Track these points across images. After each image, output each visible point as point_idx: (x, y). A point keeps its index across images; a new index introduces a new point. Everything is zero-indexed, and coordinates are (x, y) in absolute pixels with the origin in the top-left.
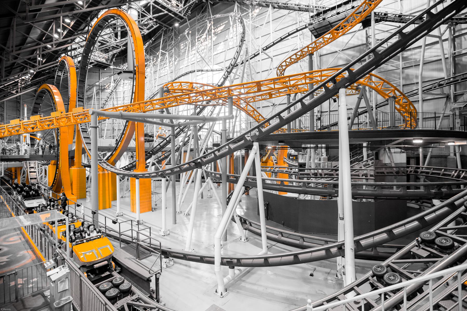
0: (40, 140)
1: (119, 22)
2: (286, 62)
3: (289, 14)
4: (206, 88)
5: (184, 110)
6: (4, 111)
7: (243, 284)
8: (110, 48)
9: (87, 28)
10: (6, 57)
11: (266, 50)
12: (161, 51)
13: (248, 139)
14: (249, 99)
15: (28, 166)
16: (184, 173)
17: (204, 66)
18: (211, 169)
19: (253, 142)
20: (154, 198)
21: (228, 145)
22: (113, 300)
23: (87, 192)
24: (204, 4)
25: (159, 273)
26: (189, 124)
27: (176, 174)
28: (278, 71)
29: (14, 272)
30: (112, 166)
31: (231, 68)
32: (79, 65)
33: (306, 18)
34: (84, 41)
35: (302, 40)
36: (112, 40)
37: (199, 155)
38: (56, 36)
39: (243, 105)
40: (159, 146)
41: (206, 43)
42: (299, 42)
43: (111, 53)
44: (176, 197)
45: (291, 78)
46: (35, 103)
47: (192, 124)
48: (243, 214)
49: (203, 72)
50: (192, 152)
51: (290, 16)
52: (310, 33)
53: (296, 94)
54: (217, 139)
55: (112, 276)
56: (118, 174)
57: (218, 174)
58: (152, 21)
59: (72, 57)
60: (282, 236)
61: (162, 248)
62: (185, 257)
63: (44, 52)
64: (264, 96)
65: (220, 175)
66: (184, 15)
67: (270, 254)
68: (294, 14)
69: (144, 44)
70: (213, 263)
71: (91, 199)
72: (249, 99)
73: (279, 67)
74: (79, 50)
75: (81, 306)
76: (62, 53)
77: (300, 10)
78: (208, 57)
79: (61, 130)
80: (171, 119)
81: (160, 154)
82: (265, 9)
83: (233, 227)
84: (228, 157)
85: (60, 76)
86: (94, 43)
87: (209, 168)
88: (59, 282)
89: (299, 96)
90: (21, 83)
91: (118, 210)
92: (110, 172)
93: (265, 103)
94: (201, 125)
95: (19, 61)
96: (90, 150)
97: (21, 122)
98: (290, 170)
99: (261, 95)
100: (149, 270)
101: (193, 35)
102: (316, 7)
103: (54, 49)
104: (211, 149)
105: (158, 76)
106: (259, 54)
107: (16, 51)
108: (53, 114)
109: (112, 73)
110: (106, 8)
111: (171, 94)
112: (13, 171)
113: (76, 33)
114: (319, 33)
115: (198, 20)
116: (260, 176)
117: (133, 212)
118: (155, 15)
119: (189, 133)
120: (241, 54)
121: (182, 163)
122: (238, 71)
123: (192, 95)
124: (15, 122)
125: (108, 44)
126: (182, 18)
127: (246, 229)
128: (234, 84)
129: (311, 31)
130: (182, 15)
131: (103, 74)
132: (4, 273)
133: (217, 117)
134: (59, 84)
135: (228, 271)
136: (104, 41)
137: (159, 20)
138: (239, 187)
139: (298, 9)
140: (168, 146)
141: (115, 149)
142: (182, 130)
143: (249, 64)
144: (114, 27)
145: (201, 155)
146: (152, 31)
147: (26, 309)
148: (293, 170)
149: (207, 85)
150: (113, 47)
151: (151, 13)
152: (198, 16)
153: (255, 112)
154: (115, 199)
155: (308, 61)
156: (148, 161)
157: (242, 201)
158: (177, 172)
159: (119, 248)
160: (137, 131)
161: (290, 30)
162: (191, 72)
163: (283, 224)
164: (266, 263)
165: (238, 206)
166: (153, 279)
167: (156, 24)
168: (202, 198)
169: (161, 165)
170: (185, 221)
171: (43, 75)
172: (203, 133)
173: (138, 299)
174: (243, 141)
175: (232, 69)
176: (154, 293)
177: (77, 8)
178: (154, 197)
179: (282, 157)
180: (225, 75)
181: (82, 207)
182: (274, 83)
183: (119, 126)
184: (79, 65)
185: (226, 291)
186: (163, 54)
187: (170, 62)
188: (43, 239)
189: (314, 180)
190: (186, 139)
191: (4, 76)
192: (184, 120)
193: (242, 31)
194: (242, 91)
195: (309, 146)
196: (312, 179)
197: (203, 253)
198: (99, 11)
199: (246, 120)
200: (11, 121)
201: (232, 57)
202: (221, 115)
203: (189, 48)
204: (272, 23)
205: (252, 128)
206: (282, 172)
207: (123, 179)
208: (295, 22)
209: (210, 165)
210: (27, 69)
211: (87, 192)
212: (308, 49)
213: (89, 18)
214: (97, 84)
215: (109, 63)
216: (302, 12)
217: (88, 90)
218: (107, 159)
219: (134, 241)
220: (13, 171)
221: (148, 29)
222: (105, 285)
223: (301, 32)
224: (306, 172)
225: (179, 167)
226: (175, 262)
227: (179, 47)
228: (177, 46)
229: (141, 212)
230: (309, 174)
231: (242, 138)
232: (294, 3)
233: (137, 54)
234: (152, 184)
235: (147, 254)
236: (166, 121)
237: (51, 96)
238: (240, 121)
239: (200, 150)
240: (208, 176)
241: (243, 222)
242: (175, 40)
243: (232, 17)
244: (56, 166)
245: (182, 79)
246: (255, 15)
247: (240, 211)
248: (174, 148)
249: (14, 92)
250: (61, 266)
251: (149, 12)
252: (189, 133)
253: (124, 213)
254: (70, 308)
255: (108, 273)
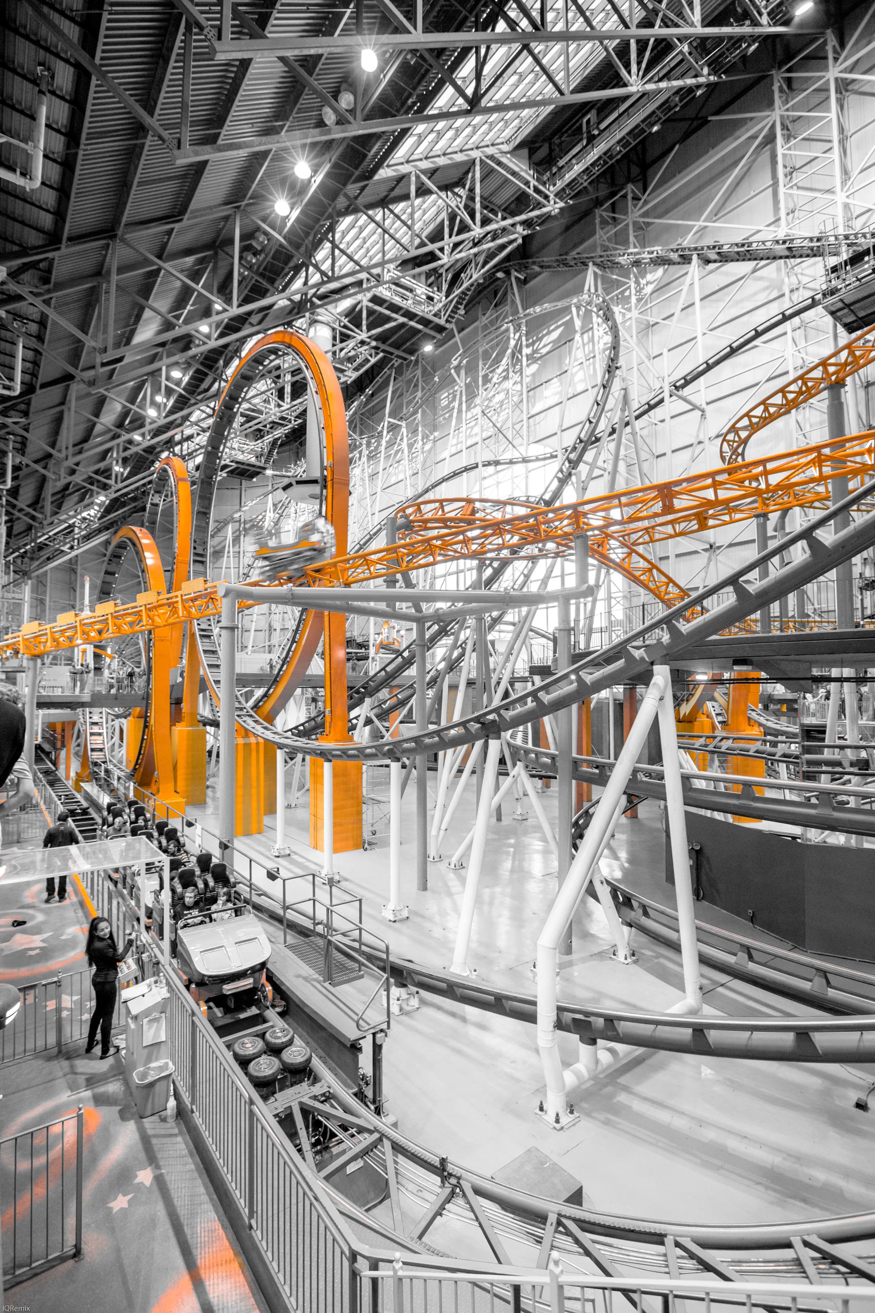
0: (112, 658)
1: (288, 362)
2: (750, 417)
3: (754, 271)
4: (511, 512)
5: (449, 577)
6: (45, 592)
7: (623, 1098)
8: (265, 426)
9: (216, 385)
10: (54, 473)
11: (683, 386)
12: (387, 419)
13: (637, 654)
14: (634, 537)
15: (88, 720)
16: (450, 751)
17: (502, 448)
18: (525, 740)
19: (652, 664)
20: (368, 814)
21: (576, 671)
22: (266, 1087)
23: (208, 787)
24: (499, 282)
25: (382, 1031)
26: (463, 613)
27: (426, 753)
28: (725, 447)
29: (55, 979)
30: (266, 724)
31: (579, 450)
32: (197, 474)
33: (813, 274)
34: (210, 416)
35: (802, 344)
36: (272, 406)
37: (490, 700)
38: (152, 413)
39: (617, 553)
40: (383, 673)
41: (508, 384)
42: (790, 349)
43: (268, 439)
44: (429, 813)
45: (770, 466)
46: (107, 573)
47: (471, 612)
48: (618, 874)
49: (499, 467)
50: (470, 690)
51: (761, 279)
52: (829, 319)
53: (785, 512)
54: (542, 652)
55: (265, 1021)
56: (281, 746)
57: (547, 755)
58: (366, 347)
59: (183, 457)
60: (751, 958)
61: (391, 959)
62: (451, 990)
63: (127, 454)
64: (683, 525)
65: (553, 758)
66: (447, 321)
67: (710, 1014)
68: (771, 270)
69: (347, 407)
70: (531, 1018)
71: (216, 808)
72: (634, 537)
73: (728, 432)
74: (197, 440)
75: (193, 1088)
76: (162, 451)
77: (792, 253)
78: (514, 424)
79: (158, 633)
80: (416, 601)
81: (384, 693)
82: (676, 271)
83: (589, 915)
84: (575, 707)
85: (157, 505)
86: (230, 422)
87: (520, 736)
88: (145, 1021)
89: (798, 520)
90: (79, 528)
91: (279, 843)
92: (261, 740)
93: (685, 544)
94: (495, 614)
95: (78, 479)
96: (217, 682)
97: (78, 619)
98: (768, 748)
99: (672, 522)
100: (356, 1018)
101: (471, 369)
102: (847, 237)
103: (148, 442)
104: (524, 680)
105: (380, 485)
106: (662, 401)
107: (75, 455)
108: (143, 599)
109: (270, 488)
110: (258, 333)
111: (416, 532)
112: (59, 729)
113: (193, 401)
114: (861, 314)
115: (485, 327)
116: (675, 763)
117: (316, 847)
118: (374, 332)
119: (462, 637)
120: (607, 408)
121: (444, 723)
122: (602, 455)
123: (470, 534)
124: (65, 619)
125: (262, 417)
126: (440, 329)
127: (630, 925)
128: (588, 496)
129: (832, 313)
130: (442, 322)
131: (248, 491)
132: (36, 978)
133: (542, 592)
134: (154, 523)
135: (576, 1052)
136: (253, 411)
137: (384, 343)
138: (610, 797)
139: (787, 253)
140: (406, 673)
141: (275, 681)
142: (443, 632)
143: (634, 433)
144: (276, 374)
145: (497, 702)
146: (366, 372)
147: (76, 1074)
148: (781, 748)
149: (512, 502)
150: (273, 422)
151: (364, 328)
152: (484, 318)
153: (655, 571)
154: (271, 809)
155: (825, 405)
156: (353, 714)
157: (617, 836)
158: (432, 746)
159: (282, 946)
160: (327, 633)
161: (760, 318)
162: (466, 469)
163: (752, 920)
164: (698, 1042)
165: (606, 852)
166: (367, 1045)
167: (377, 354)
168: (499, 819)
169: (386, 724)
170: (450, 884)
171: (124, 504)
172: (502, 636)
173: (328, 1097)
174: (621, 663)
175: (584, 450)
176: (367, 1084)
177: (197, 342)
178: (370, 813)
179: (754, 714)
180: (561, 471)
181: (198, 827)
182: (716, 485)
183: (283, 620)
184: (197, 474)
185: (572, 1112)
186: (393, 428)
187: (410, 446)
188: (115, 903)
189: (855, 784)
190: (456, 654)
191: (48, 514)
192: (449, 604)
193: (608, 339)
194: (616, 514)
195: (835, 672)
196: (846, 777)
197: (500, 984)
198: (243, 341)
199: (625, 597)
200: (59, 617)
201: (584, 418)
202: (554, 585)
203: (460, 404)
204: (702, 307)
205: (647, 624)
206: (744, 753)
207: (292, 759)
208: (775, 294)
209: (521, 728)
210: (91, 496)
211: (208, 787)
212: (825, 371)
213: (221, 362)
214: (236, 515)
215: (262, 465)
216: (799, 260)
217: (216, 533)
218: (256, 707)
219: (320, 929)
220: (59, 730)
221: (356, 369)
222: (249, 1045)
223: (796, 320)
224: (827, 754)
225: (437, 733)
226: (423, 1002)
227: (434, 407)
228: (431, 401)
229: (336, 850)
230: (839, 764)
231: (618, 652)
232: (770, 237)
233: (330, 436)
234: (364, 775)
235: (352, 970)
236: (403, 607)
237: (137, 553)
238: (609, 598)
239: (493, 682)
240: (515, 759)
241: (623, 902)
242: (423, 389)
243: (578, 308)
244: (142, 721)
245: (443, 491)
246: (649, 289)
247: (610, 866)
248: (424, 678)
249: (65, 548)
250: (153, 979)
251: (359, 326)
252: (462, 637)
253: (293, 849)
254: (168, 1090)
255: (254, 1011)
